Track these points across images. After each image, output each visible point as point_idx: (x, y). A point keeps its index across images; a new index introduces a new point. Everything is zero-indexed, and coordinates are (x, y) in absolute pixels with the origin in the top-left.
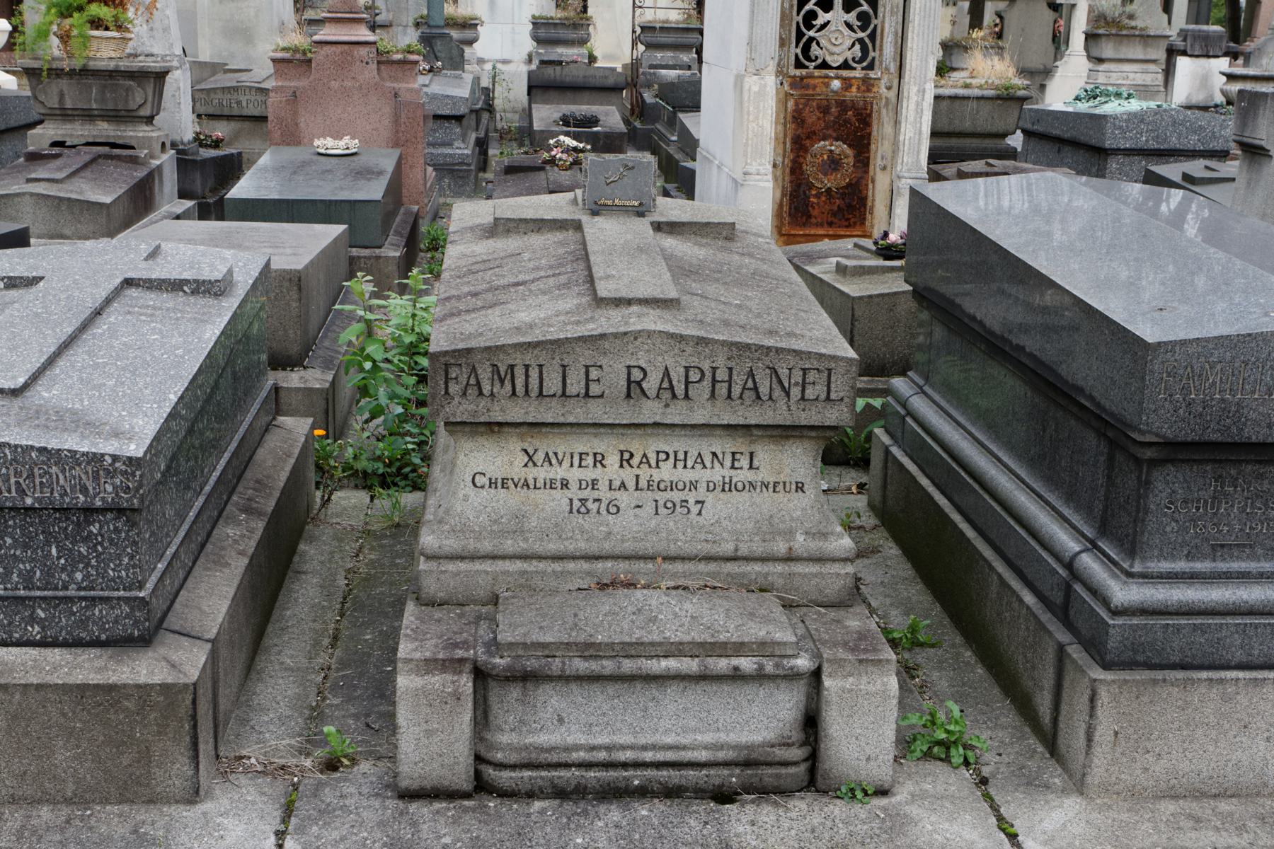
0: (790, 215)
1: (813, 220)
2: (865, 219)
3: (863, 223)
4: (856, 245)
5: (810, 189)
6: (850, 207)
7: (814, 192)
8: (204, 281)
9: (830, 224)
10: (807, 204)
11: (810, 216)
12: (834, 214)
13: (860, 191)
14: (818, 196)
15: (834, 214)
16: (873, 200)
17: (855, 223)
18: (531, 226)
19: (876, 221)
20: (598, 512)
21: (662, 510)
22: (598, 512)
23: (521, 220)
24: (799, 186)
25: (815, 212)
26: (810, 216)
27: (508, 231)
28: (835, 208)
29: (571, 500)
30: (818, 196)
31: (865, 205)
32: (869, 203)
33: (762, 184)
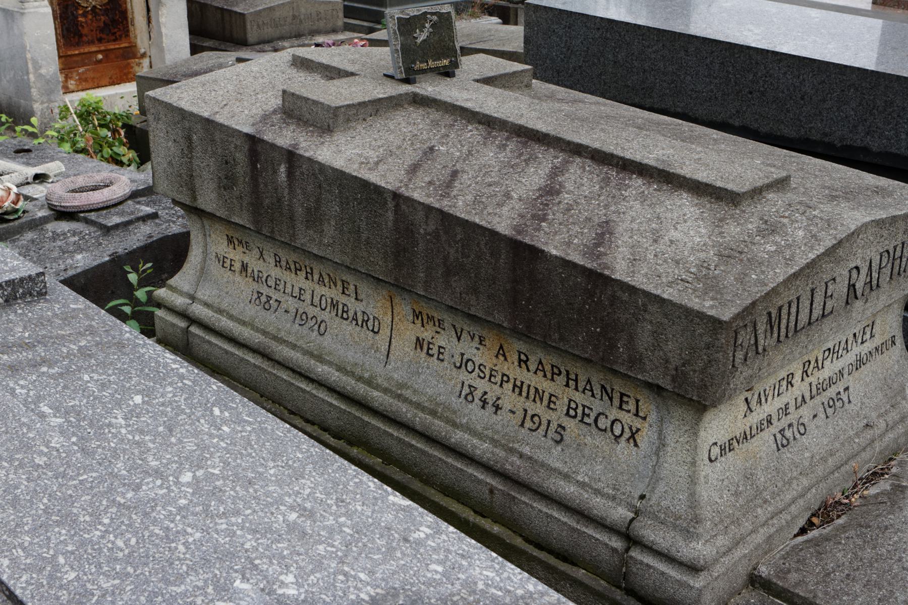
0: (63, 37)
1: (85, 39)
2: (128, 31)
3: (127, 36)
4: (302, 64)
5: (77, 9)
6: (114, 22)
7: (81, 12)
8: (22, 280)
9: (100, 40)
10: (76, 24)
11: (81, 36)
12: (102, 31)
13: (120, 6)
14: (85, 15)
15: (102, 31)
16: (133, 12)
17: (121, 36)
18: (370, 109)
19: (138, 32)
20: (795, 438)
21: (528, 424)
22: (795, 438)
23: (360, 104)
24: (66, 7)
25: (85, 31)
26: (81, 36)
27: (348, 120)
28: (102, 25)
29: (775, 435)
30: (85, 15)
31: (126, 18)
32: (130, 16)
33: (42, 10)
